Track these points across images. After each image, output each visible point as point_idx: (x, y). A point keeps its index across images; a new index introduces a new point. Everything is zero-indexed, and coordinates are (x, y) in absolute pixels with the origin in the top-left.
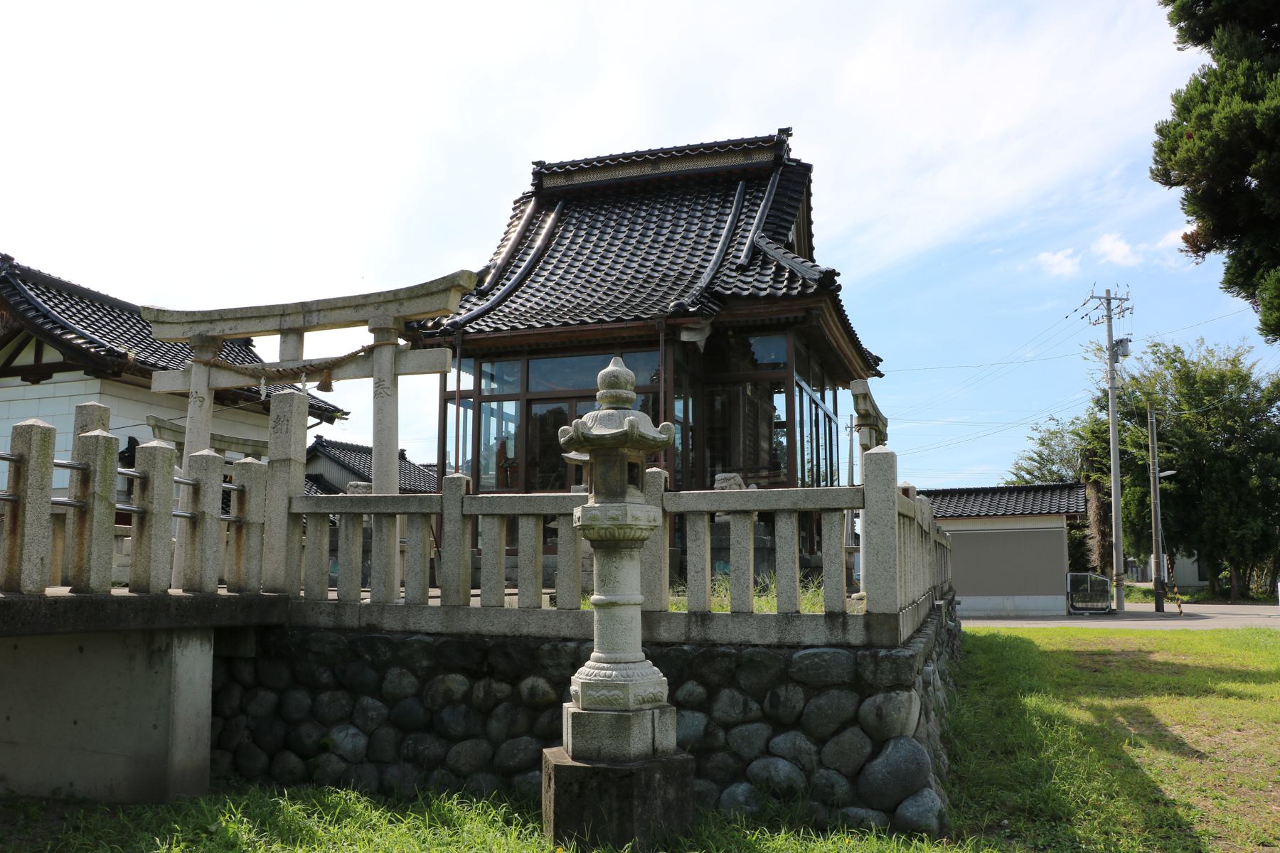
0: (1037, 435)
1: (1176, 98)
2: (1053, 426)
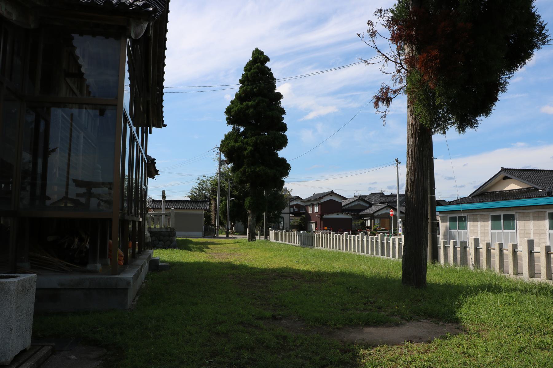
0: (199, 182)
1: (225, 135)
2: (204, 179)
